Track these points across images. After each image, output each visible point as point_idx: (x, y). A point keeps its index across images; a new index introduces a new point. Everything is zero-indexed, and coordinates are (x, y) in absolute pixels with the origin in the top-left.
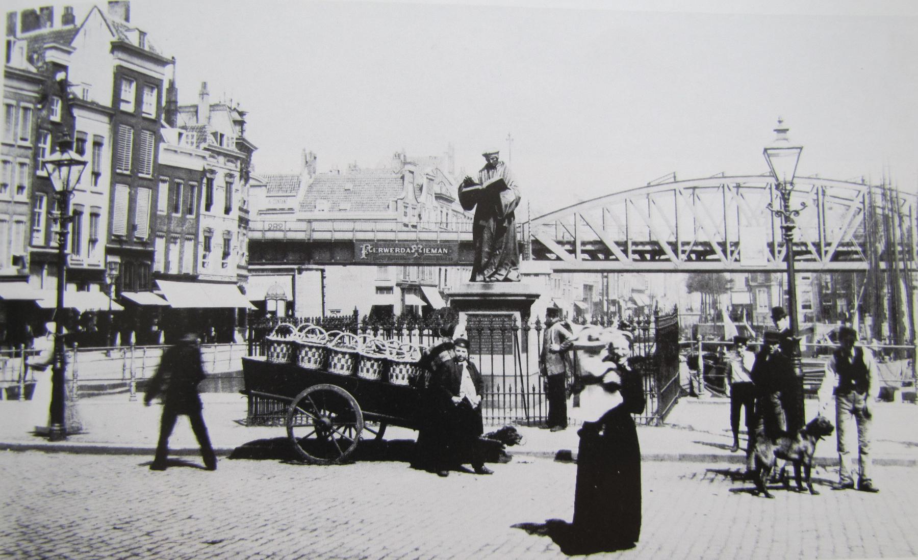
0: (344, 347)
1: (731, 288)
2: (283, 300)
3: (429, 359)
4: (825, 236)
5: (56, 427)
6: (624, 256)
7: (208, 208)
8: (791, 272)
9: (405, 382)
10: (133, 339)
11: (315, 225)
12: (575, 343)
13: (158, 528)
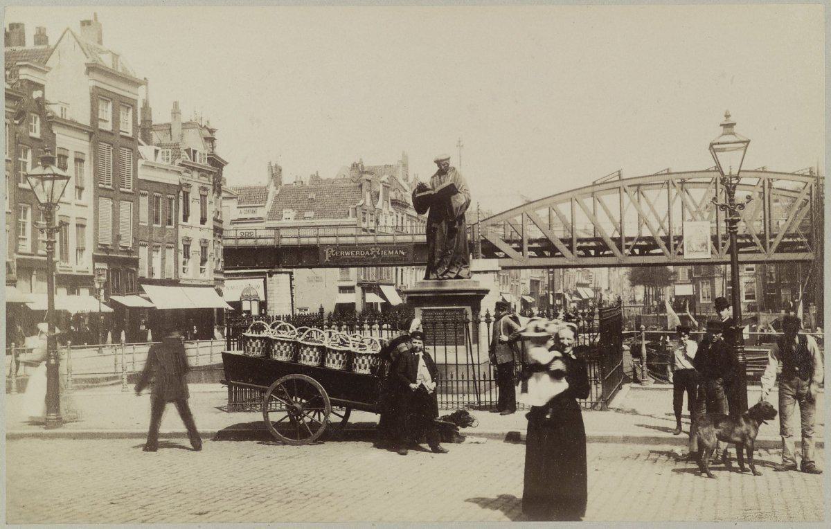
0: (311, 341)
1: (674, 281)
2: (257, 300)
3: (389, 350)
4: (770, 228)
5: (53, 416)
6: (569, 252)
7: (185, 219)
8: (735, 264)
9: (367, 372)
10: (123, 338)
11: (283, 232)
12: (524, 334)
13: (152, 502)
